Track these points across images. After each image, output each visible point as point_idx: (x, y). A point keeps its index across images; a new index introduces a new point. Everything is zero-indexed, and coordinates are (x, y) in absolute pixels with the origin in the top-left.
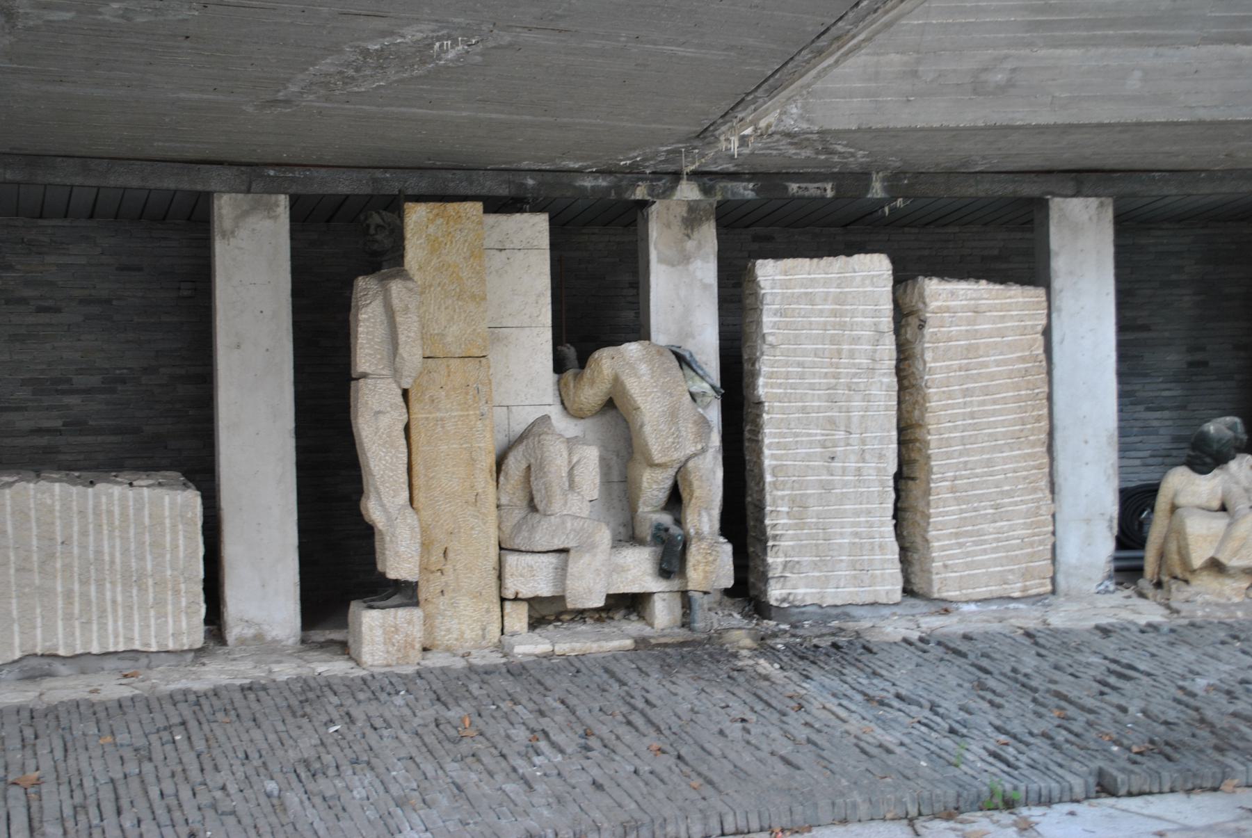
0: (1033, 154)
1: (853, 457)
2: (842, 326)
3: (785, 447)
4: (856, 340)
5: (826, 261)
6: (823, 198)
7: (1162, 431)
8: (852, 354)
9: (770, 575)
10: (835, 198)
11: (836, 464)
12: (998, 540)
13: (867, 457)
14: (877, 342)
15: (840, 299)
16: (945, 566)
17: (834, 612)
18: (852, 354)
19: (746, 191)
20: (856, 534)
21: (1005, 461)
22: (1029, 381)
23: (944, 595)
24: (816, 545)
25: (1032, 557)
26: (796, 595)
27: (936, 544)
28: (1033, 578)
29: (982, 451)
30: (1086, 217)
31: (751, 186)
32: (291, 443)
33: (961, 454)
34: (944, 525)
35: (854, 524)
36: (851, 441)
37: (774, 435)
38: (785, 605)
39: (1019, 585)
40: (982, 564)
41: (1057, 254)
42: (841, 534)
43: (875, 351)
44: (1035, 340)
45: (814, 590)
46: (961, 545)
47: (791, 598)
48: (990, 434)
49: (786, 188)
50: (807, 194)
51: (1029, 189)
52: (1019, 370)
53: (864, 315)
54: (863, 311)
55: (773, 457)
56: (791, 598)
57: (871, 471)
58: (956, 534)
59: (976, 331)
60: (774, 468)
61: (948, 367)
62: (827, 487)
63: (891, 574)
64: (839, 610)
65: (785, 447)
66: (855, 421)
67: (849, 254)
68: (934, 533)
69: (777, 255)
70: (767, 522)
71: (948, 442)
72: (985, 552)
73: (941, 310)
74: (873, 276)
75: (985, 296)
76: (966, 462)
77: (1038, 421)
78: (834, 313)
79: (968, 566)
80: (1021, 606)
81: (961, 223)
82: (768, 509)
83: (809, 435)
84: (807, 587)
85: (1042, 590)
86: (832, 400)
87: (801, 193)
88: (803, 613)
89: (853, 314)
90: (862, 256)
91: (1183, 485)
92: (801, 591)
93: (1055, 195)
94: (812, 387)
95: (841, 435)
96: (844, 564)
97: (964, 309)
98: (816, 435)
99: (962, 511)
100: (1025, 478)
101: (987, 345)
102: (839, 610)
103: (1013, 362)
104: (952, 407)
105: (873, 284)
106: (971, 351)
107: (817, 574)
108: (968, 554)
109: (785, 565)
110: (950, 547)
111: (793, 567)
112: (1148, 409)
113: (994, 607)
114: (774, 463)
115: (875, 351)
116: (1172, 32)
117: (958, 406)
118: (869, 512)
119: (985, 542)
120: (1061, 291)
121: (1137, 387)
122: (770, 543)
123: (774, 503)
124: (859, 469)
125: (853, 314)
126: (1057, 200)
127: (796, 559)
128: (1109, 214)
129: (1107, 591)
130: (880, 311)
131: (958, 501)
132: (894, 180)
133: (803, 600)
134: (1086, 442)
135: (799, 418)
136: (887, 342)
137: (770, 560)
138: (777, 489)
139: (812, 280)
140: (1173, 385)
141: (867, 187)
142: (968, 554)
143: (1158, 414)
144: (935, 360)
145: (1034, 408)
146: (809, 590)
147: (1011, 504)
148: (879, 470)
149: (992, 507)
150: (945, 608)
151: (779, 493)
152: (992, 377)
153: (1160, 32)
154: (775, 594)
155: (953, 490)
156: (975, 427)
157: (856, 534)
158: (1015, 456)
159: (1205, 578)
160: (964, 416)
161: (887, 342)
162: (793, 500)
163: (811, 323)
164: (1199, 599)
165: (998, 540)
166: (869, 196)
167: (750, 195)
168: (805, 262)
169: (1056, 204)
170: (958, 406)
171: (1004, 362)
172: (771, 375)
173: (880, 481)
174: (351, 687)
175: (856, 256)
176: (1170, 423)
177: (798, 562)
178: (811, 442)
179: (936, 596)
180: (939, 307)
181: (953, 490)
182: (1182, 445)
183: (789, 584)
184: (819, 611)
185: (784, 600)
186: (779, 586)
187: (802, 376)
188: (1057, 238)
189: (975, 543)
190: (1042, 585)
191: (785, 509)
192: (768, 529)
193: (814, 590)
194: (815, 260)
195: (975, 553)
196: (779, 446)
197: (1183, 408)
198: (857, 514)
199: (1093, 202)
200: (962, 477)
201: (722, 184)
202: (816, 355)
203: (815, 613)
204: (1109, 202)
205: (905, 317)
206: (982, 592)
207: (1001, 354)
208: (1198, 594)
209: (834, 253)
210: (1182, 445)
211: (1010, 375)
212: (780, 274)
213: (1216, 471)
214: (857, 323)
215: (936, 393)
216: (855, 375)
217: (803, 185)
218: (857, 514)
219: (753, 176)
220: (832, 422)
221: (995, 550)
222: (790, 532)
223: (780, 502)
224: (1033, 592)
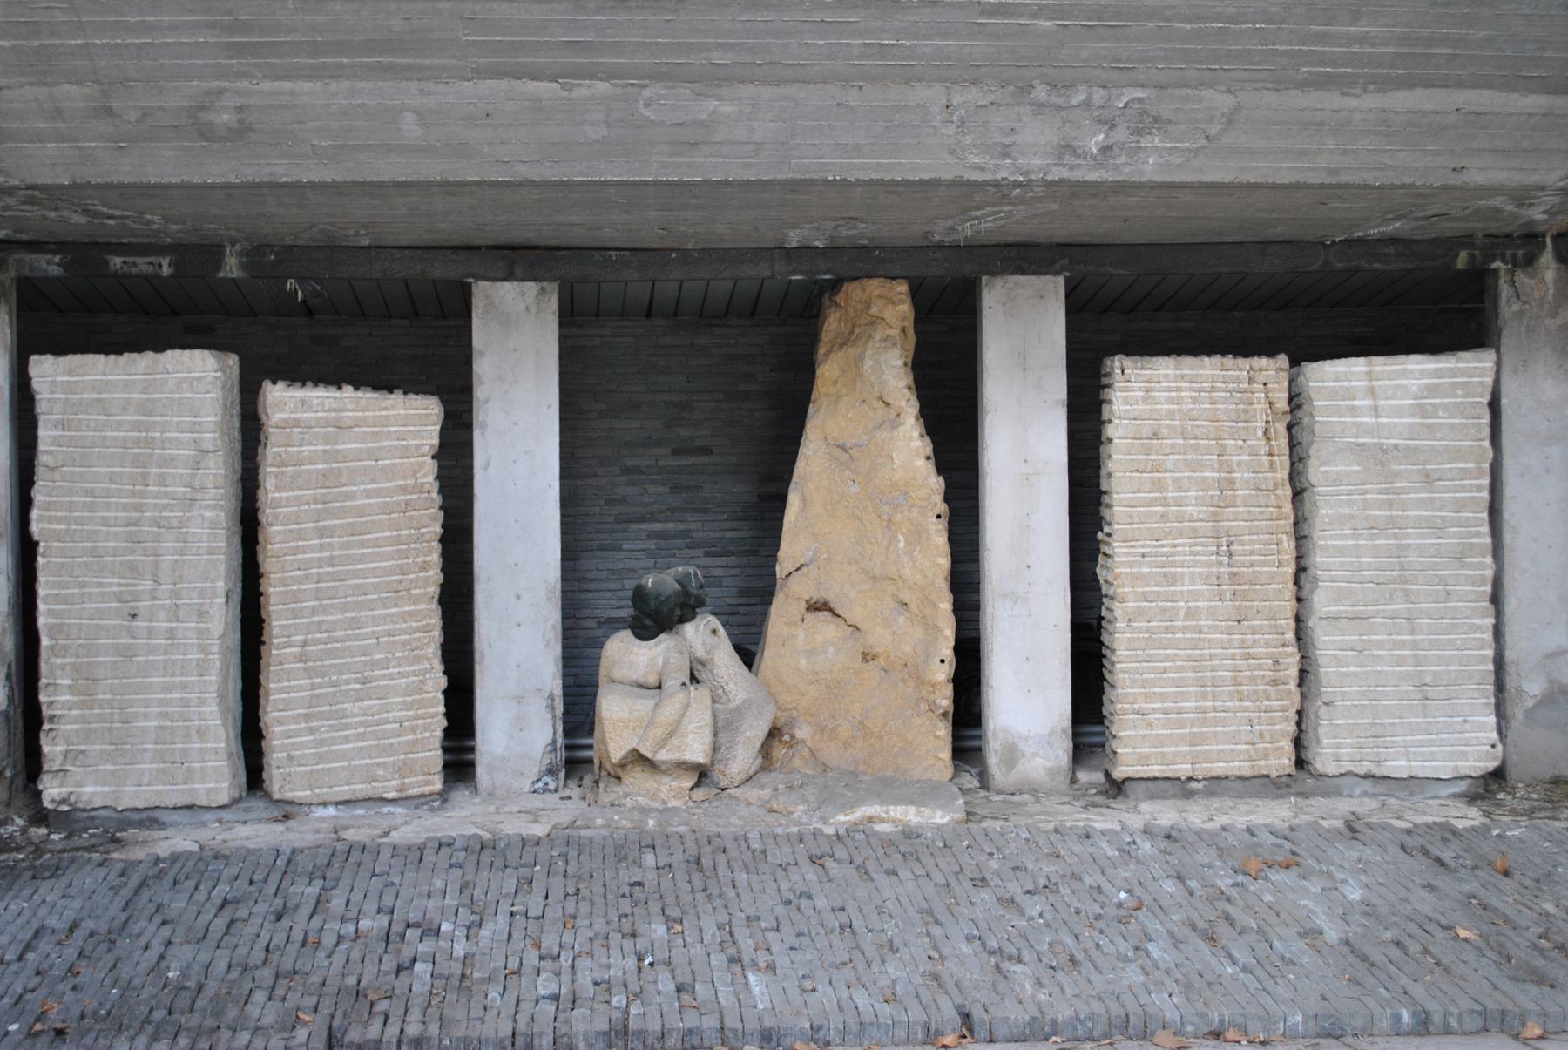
0: (453, 223)
1: (162, 615)
2: (150, 443)
3: (66, 600)
4: (169, 462)
5: (127, 357)
6: (158, 276)
7: (725, 582)
8: (161, 480)
9: (46, 768)
10: (172, 276)
11: (139, 624)
12: (364, 724)
13: (182, 614)
14: (197, 465)
15: (145, 408)
16: (290, 758)
17: (136, 817)
18: (161, 480)
19: (50, 266)
20: (165, 715)
21: (376, 621)
22: (411, 518)
23: (289, 795)
24: (110, 730)
25: (413, 746)
26: (79, 795)
27: (278, 729)
28: (414, 773)
29: (345, 607)
30: (522, 306)
31: (57, 259)
32: (476, 570)
33: (314, 611)
34: (288, 705)
35: (162, 703)
36: (159, 594)
37: (52, 585)
38: (66, 808)
39: (394, 783)
40: (343, 756)
41: (482, 354)
42: (145, 715)
43: (193, 476)
44: (421, 465)
45: (106, 789)
46: (312, 731)
47: (73, 799)
48: (357, 587)
49: (106, 263)
50: (134, 271)
51: (441, 270)
52: (398, 503)
53: (179, 427)
54: (178, 424)
55: (51, 613)
56: (73, 799)
57: (189, 634)
58: (307, 715)
59: (337, 451)
60: (51, 628)
61: (296, 498)
62: (127, 653)
63: (215, 768)
64: (144, 815)
65: (66, 600)
66: (165, 566)
67: (160, 348)
68: (276, 714)
69: (60, 350)
70: (42, 698)
71: (296, 597)
72: (346, 739)
73: (285, 424)
74: (193, 379)
75: (350, 407)
76: (320, 623)
77: (423, 569)
78: (137, 427)
79: (320, 758)
80: (400, 810)
81: (353, 308)
82: (43, 681)
83: (100, 585)
84: (97, 784)
85: (427, 789)
86: (133, 539)
87: (126, 268)
88: (93, 818)
89: (164, 428)
90: (178, 352)
91: (627, 656)
92: (89, 789)
93: (478, 278)
94: (105, 522)
95: (147, 585)
96: (148, 755)
97: (319, 423)
98: (111, 585)
99: (313, 687)
100: (404, 644)
101: (353, 470)
102: (144, 815)
103: (389, 492)
104: (304, 550)
105: (192, 389)
106: (328, 478)
107: (110, 767)
108: (322, 743)
109: (66, 754)
110: (296, 734)
111: (76, 757)
112: (707, 554)
113: (361, 812)
114: (52, 621)
115: (193, 476)
116: (427, 62)
117: (312, 549)
118: (184, 687)
119: (347, 726)
120: (487, 401)
121: (693, 526)
122: (46, 726)
123: (51, 675)
124: (171, 630)
125: (164, 428)
126: (482, 284)
127: (82, 747)
128: (553, 304)
129: (546, 790)
130: (200, 424)
131: (309, 672)
132: (255, 254)
133: (90, 802)
134: (518, 597)
135: (86, 564)
136: (212, 464)
137: (46, 749)
138: (56, 656)
139: (108, 382)
140: (741, 523)
141: (218, 262)
142: (322, 743)
143: (722, 561)
144: (278, 489)
145: (418, 553)
146: (98, 789)
147: (384, 677)
148: (200, 633)
149: (357, 681)
150: (287, 811)
151: (59, 661)
152: (360, 512)
153: (411, 61)
154: (52, 791)
155: (302, 658)
156: (333, 577)
157: (165, 715)
158: (392, 615)
159: (638, 775)
160: (320, 563)
161: (212, 464)
162: (76, 669)
163: (104, 438)
164: (629, 802)
165: (364, 724)
166: (221, 275)
167: (55, 270)
168: (99, 359)
169: (482, 291)
170: (312, 549)
171: (378, 493)
172: (47, 507)
173: (200, 646)
174: (288, 863)
175: (169, 352)
176: (595, 574)
177: (82, 752)
178: (103, 594)
179: (277, 796)
180: (285, 420)
181: (302, 658)
182: (752, 601)
183: (70, 780)
184: (115, 815)
185: (63, 801)
186: (56, 782)
187: (91, 508)
188: (481, 335)
189: (333, 728)
190: (427, 783)
191: (66, 682)
192: (44, 708)
193: (106, 789)
194: (112, 357)
195: (333, 741)
196: (58, 599)
197: (755, 553)
198: (168, 688)
199: (531, 288)
200: (317, 642)
201: (17, 257)
202: (111, 481)
203: (110, 818)
204: (553, 289)
205: (250, 431)
206: (343, 791)
207: (373, 481)
208: (627, 795)
209: (137, 347)
210: (752, 601)
211: (386, 509)
212: (64, 374)
213: (662, 636)
214: (170, 440)
215: (279, 532)
216: (165, 507)
217: (130, 259)
218: (168, 688)
219: (61, 246)
220: (133, 570)
221: (362, 737)
222: (74, 712)
223: (59, 672)
224: (416, 791)
